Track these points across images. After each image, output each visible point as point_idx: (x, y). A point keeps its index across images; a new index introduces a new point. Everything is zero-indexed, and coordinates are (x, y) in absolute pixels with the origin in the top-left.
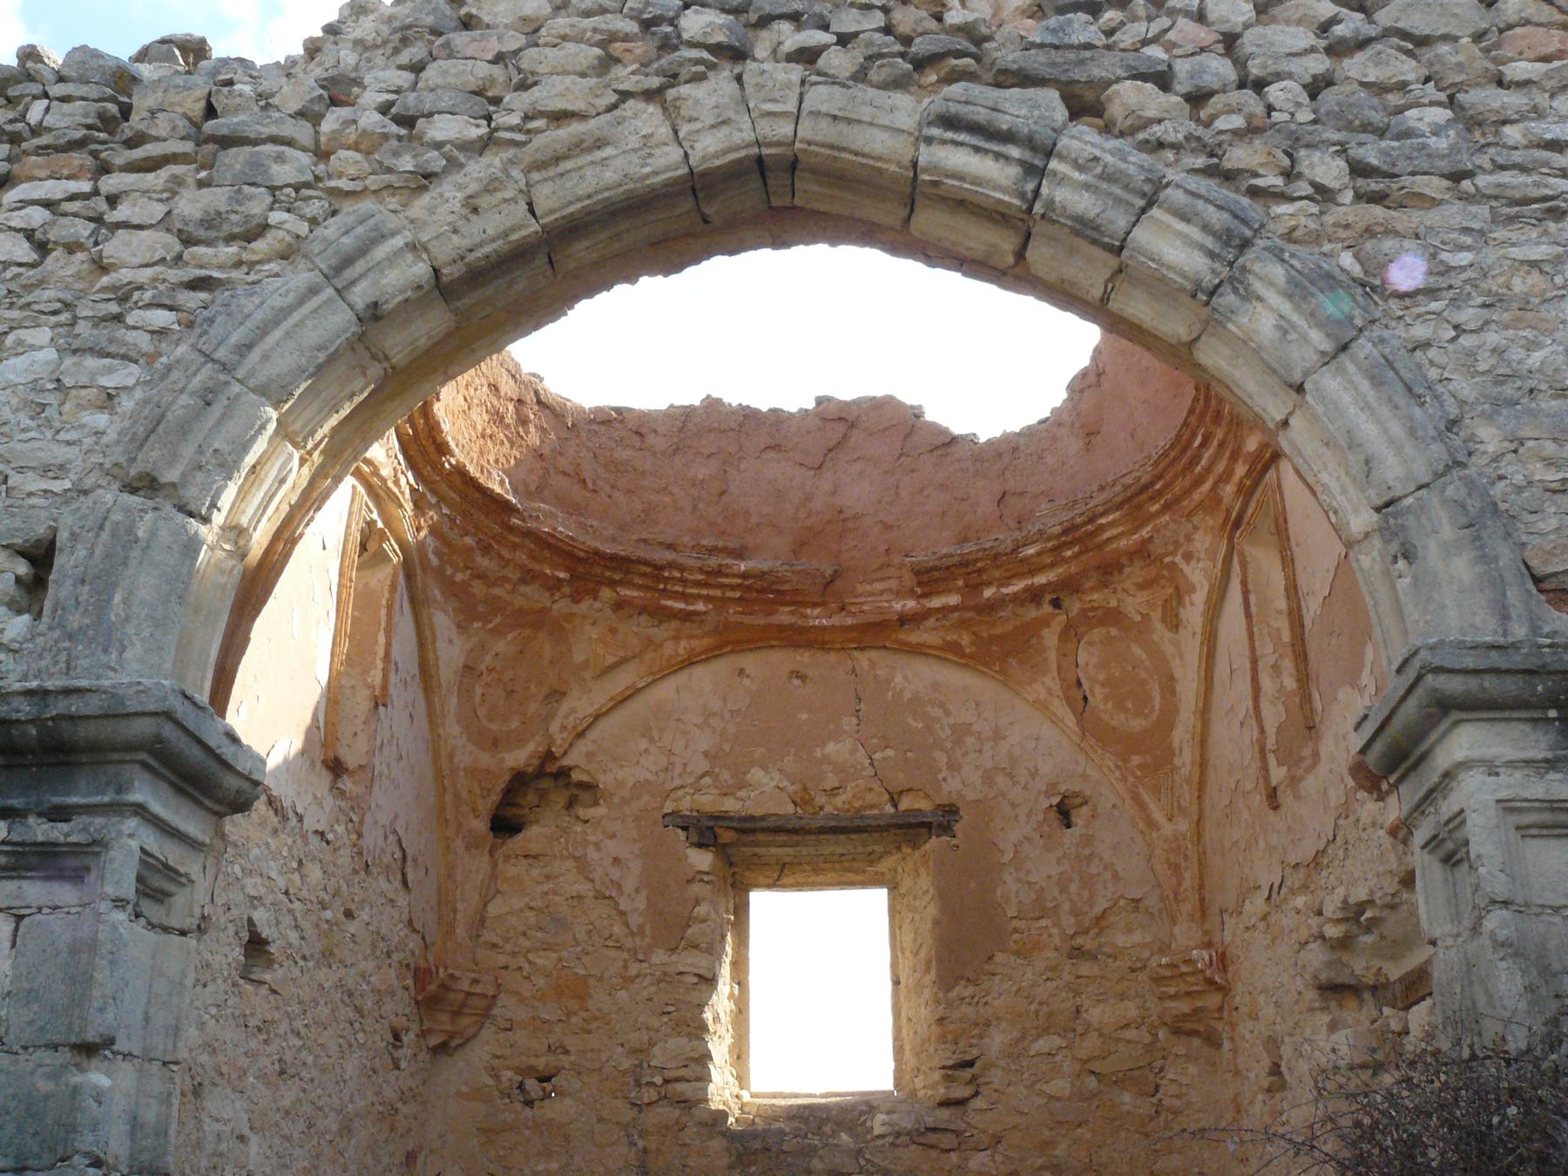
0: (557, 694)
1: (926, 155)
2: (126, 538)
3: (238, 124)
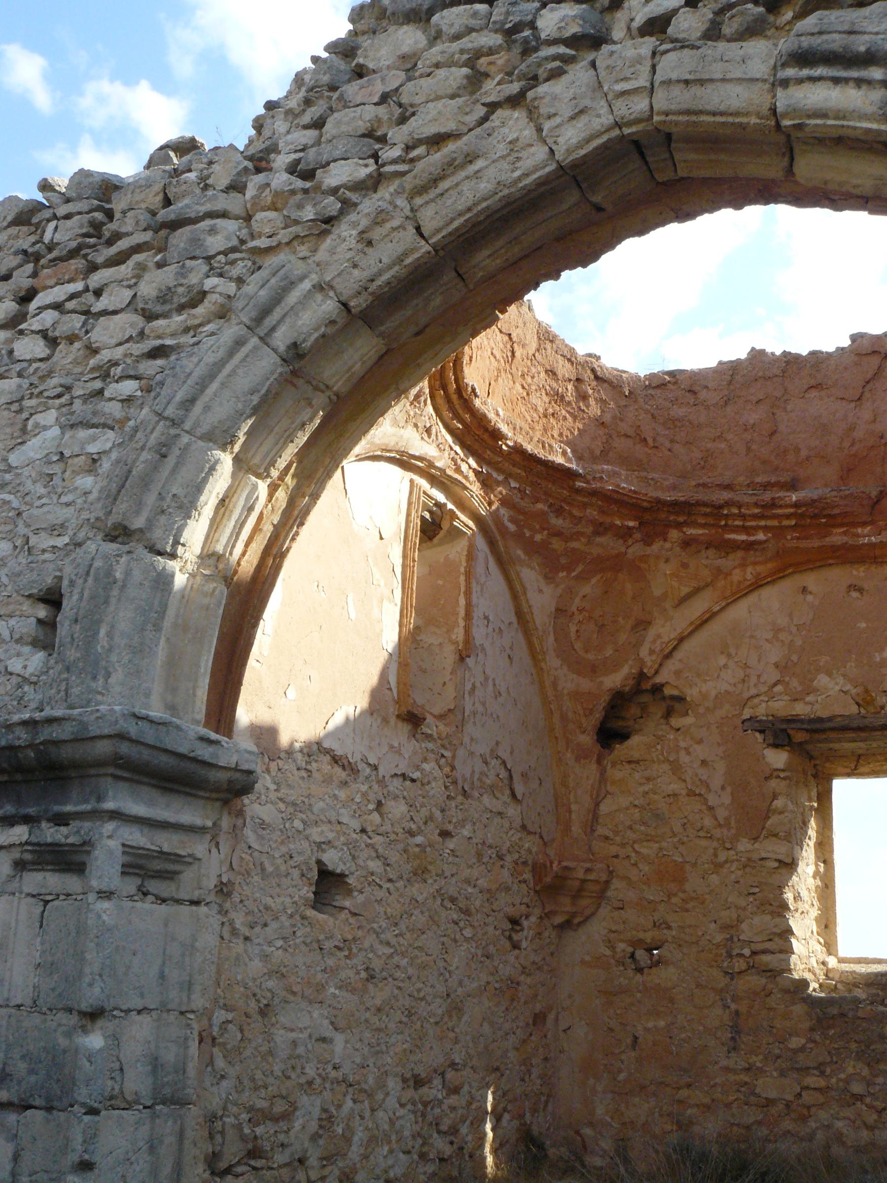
0: (643, 624)
1: (784, 99)
2: (107, 580)
3: (182, 208)
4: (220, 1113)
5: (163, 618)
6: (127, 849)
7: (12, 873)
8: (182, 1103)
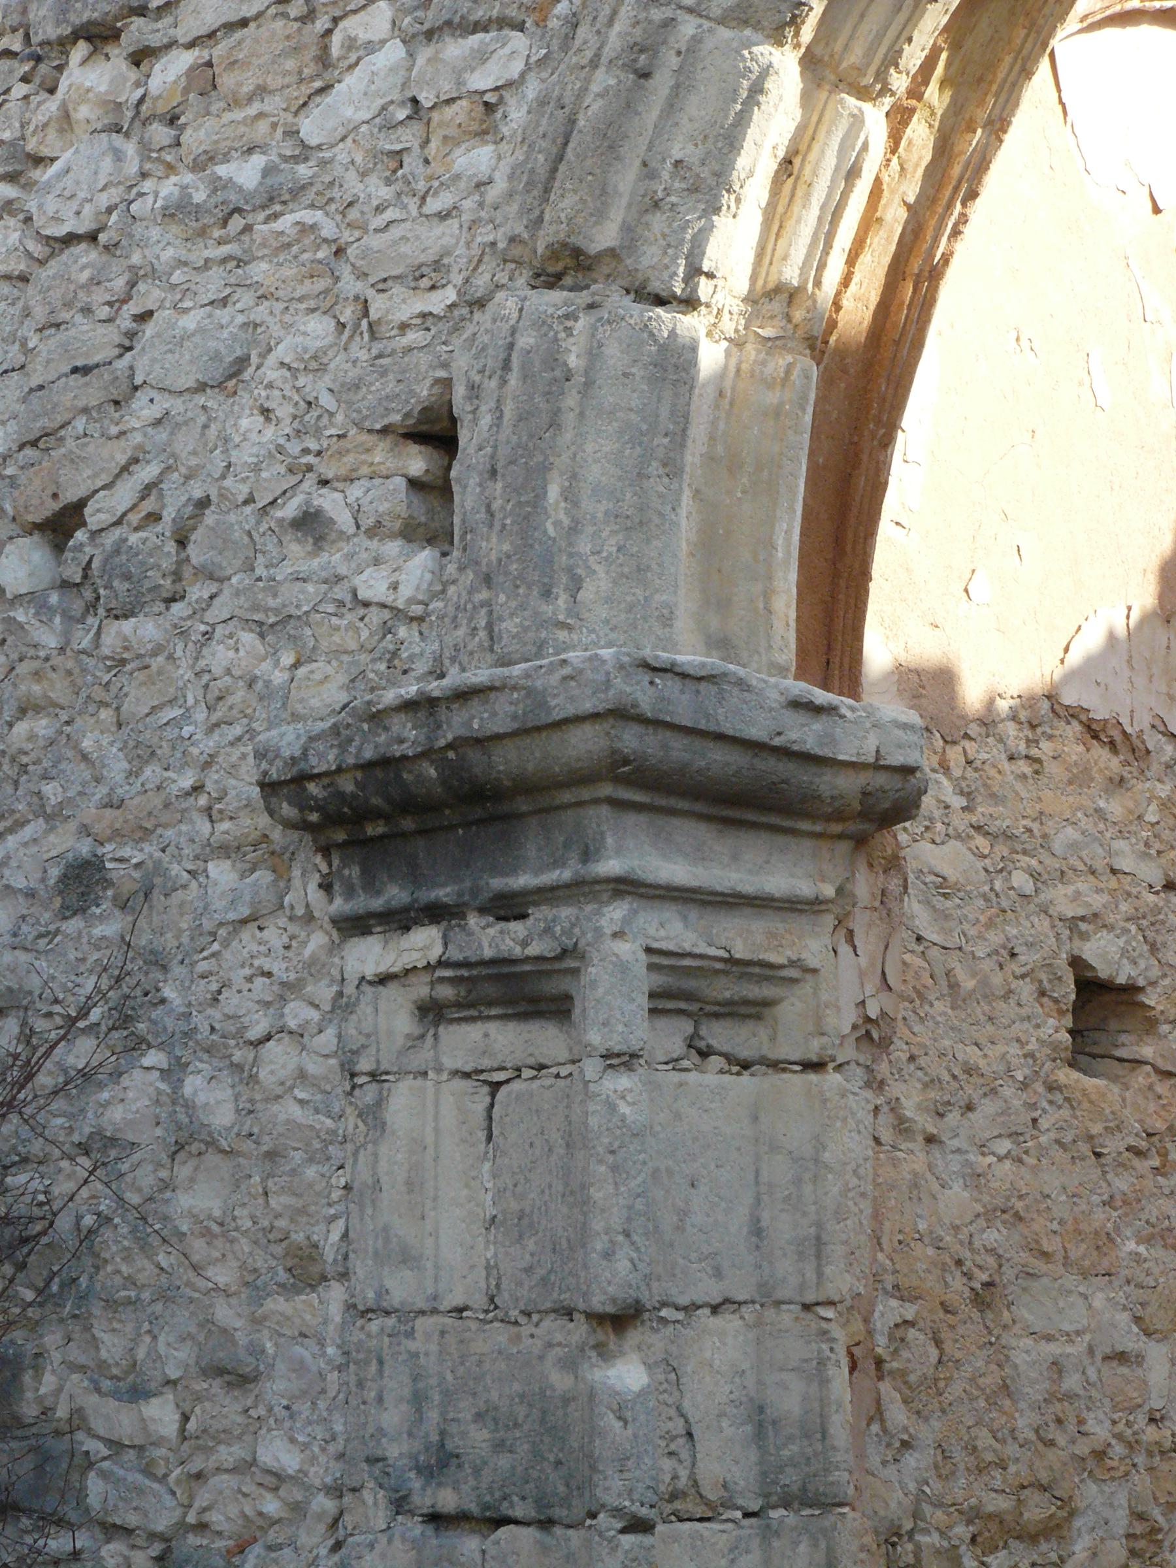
4: (908, 1525)
5: (683, 446)
6: (656, 959)
7: (417, 1031)
8: (828, 1503)
